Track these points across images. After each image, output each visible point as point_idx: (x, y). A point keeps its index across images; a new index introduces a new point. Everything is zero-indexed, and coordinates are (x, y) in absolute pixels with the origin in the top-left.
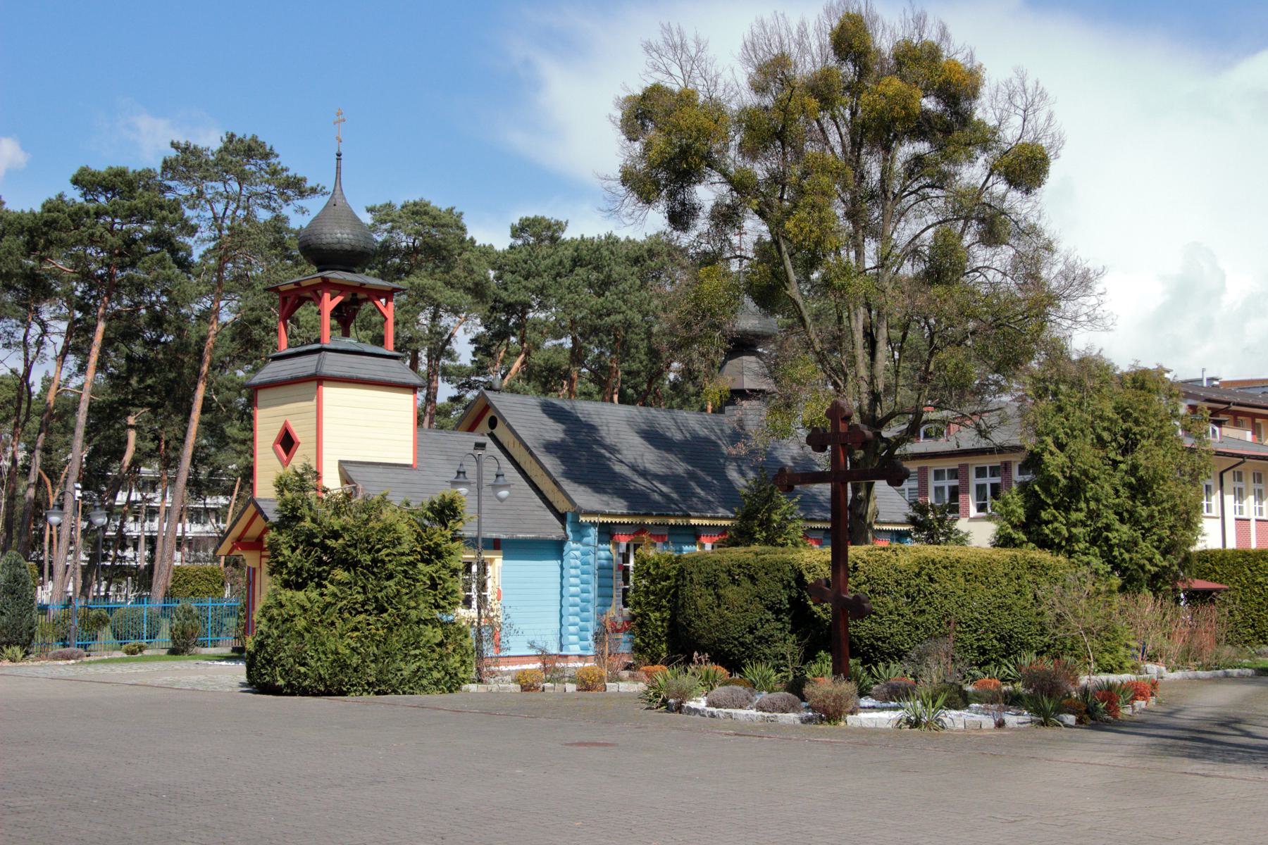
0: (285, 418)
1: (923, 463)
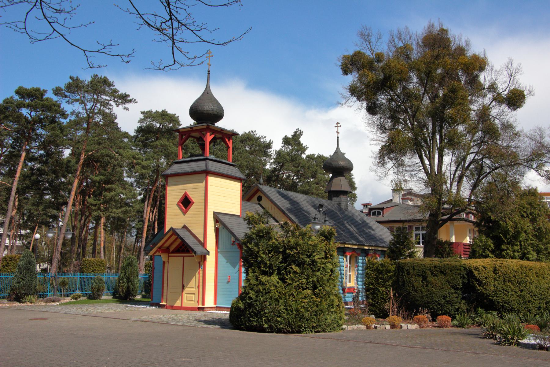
0: (184, 191)
1: (410, 224)
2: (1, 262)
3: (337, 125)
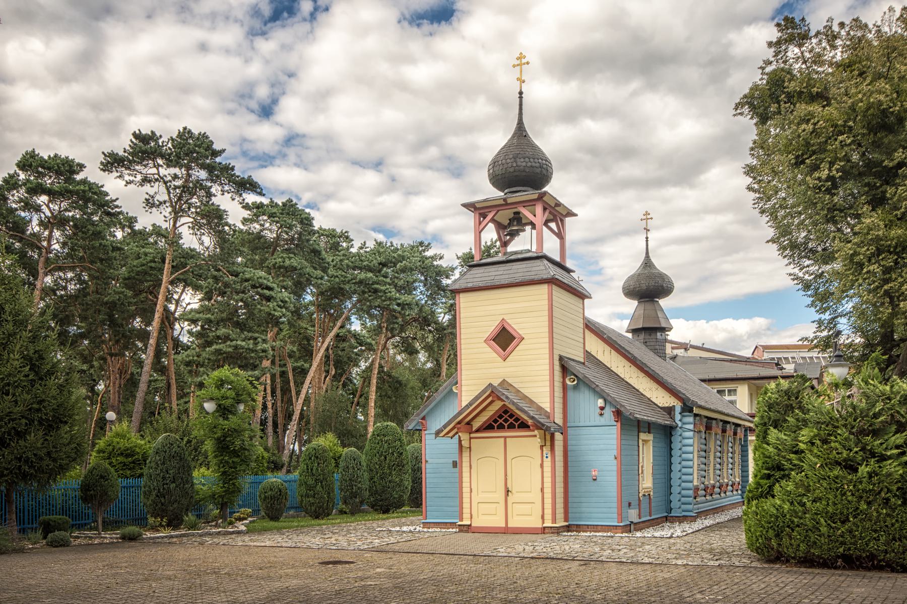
3: (645, 217)
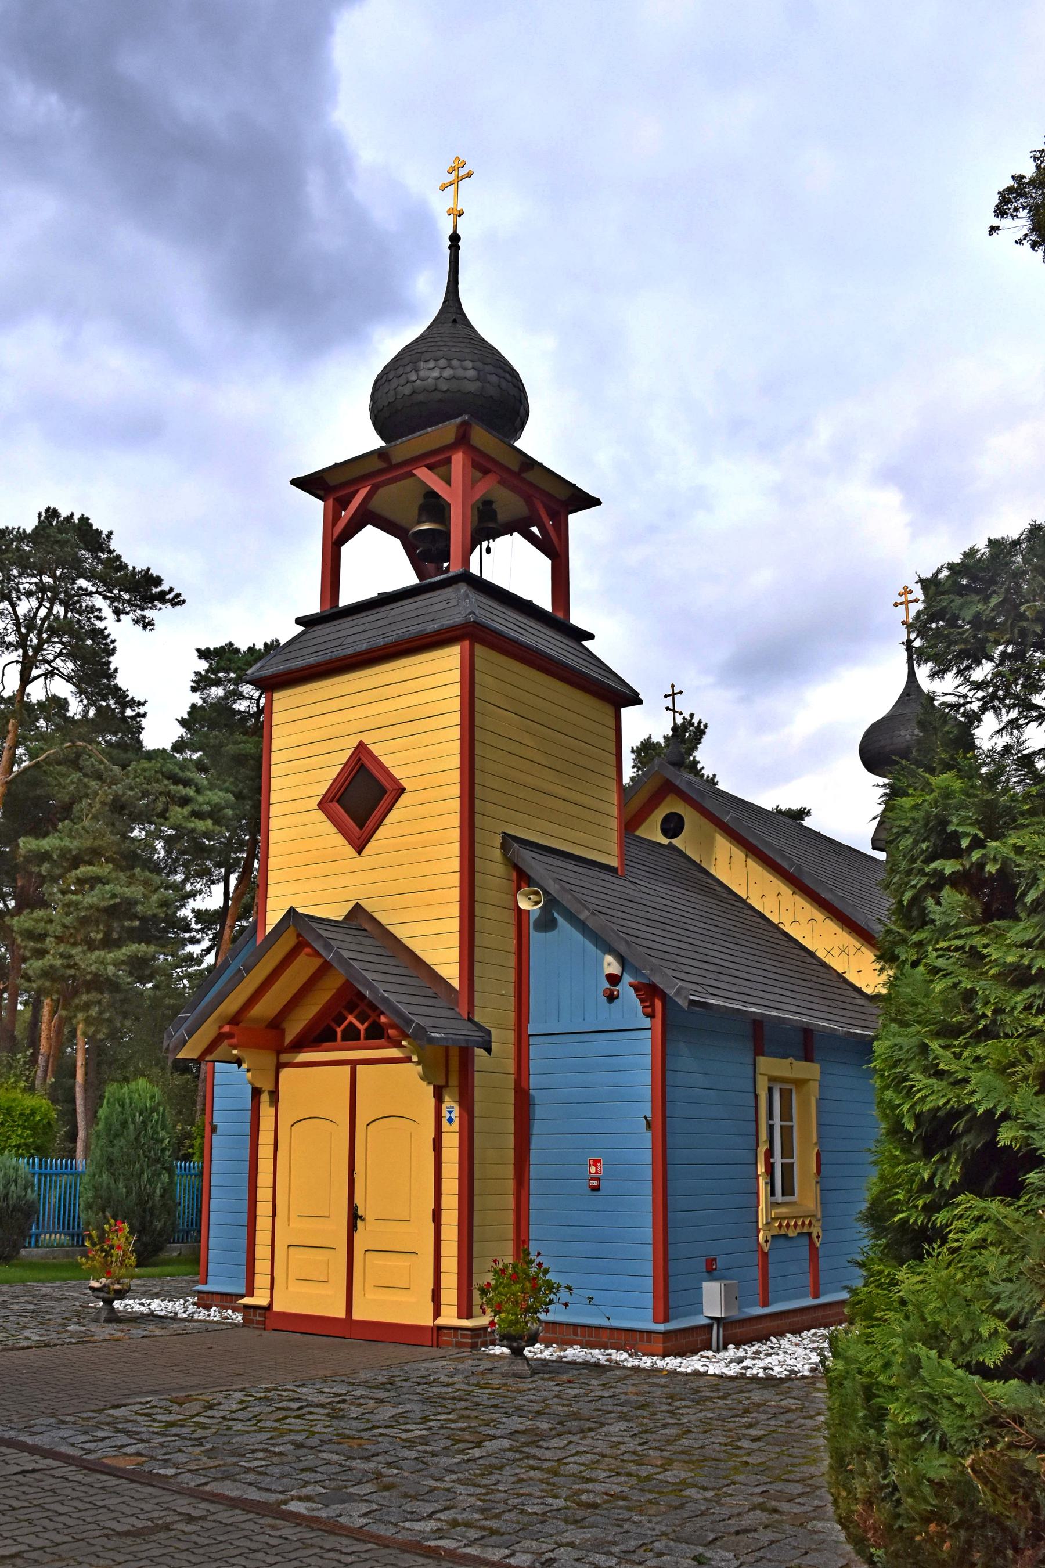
2: (719, 1556)
3: (902, 599)
